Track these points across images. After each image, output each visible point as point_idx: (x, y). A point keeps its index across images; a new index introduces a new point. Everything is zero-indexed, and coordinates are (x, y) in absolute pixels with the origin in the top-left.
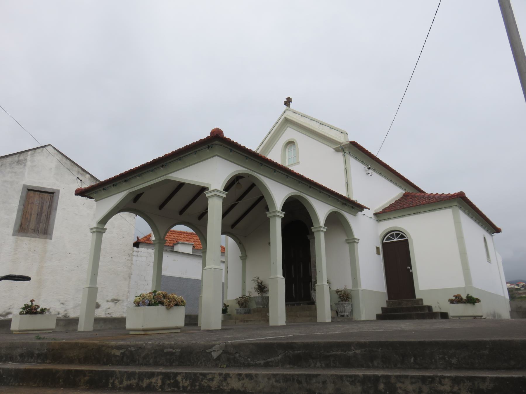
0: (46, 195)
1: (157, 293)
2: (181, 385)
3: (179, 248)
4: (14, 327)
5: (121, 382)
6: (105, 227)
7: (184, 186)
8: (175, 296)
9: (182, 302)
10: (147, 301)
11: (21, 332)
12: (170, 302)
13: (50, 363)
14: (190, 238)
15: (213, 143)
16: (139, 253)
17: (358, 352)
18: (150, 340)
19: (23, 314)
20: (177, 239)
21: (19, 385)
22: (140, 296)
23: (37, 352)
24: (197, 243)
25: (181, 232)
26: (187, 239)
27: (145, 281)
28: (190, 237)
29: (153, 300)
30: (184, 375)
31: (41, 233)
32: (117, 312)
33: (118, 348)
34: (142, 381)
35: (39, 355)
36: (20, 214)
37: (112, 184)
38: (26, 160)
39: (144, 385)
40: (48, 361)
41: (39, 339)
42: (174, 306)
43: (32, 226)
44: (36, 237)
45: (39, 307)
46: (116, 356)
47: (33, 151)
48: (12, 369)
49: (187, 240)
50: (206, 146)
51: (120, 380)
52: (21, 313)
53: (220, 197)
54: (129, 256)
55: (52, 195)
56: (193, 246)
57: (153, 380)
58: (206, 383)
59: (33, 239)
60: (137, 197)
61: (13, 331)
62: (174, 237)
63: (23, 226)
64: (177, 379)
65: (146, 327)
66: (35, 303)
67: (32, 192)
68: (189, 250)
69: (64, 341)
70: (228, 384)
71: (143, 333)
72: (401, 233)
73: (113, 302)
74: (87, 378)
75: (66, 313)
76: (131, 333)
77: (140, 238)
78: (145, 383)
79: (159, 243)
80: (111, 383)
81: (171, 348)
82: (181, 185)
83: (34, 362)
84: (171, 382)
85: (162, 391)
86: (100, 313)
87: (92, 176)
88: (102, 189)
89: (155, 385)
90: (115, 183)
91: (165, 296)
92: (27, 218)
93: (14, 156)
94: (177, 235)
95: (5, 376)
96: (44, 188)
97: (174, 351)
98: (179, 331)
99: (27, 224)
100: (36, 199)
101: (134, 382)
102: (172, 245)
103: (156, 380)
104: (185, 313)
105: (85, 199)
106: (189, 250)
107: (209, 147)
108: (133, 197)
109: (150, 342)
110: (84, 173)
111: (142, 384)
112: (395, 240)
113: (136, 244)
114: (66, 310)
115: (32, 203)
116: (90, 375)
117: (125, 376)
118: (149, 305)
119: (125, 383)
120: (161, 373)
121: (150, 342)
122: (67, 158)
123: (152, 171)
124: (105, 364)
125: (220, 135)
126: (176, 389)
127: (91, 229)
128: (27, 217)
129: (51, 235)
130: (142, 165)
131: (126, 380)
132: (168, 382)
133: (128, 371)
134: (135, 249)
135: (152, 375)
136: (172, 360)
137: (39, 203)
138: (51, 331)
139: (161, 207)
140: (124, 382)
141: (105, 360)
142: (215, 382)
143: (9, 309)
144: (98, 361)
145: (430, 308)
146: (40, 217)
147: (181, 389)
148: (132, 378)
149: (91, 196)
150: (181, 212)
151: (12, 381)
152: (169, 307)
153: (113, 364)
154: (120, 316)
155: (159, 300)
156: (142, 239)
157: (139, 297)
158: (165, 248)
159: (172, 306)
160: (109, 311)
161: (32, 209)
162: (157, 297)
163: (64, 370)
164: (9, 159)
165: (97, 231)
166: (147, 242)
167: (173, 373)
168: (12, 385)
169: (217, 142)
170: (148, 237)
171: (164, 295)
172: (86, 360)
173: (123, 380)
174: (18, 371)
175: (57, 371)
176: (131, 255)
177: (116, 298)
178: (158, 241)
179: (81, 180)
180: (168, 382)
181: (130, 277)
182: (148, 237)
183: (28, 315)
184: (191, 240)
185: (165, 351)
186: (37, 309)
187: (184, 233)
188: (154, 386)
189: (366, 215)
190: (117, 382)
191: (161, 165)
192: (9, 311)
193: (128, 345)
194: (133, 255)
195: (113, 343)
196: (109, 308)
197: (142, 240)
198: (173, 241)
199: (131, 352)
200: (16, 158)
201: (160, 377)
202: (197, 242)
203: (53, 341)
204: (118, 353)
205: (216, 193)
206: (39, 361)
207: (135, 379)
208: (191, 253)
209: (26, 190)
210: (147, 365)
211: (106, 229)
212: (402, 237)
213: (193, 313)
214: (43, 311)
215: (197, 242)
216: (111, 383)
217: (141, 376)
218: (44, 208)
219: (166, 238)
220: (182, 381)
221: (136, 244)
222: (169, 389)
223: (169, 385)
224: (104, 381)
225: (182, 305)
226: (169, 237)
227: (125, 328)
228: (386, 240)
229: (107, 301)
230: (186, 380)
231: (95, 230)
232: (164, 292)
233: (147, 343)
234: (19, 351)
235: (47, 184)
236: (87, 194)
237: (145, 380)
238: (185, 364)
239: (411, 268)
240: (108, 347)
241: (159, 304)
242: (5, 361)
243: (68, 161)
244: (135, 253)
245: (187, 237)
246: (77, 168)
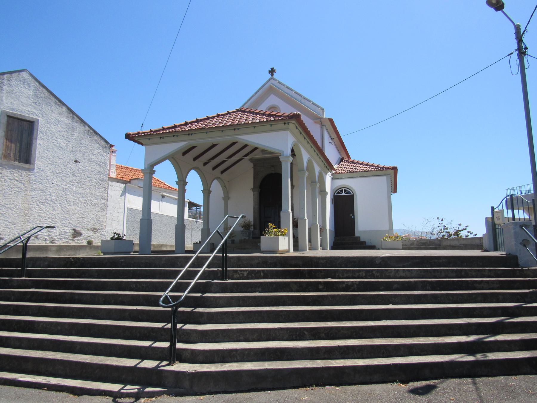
2: (375, 275)
17: (444, 260)
57: (361, 274)
58: (388, 274)
70: (398, 274)
72: (349, 190)
78: (356, 275)
89: (362, 276)
95: (269, 274)
112: (344, 194)
117: (345, 272)
122: (44, 87)
128: (8, 145)
132: (368, 274)
142: (392, 273)
145: (365, 242)
180: (368, 274)
188: (361, 276)
189: (143, 123)
201: (364, 272)
207: (351, 273)
212: (349, 193)
228: (336, 194)
230: (378, 273)
239: (354, 215)
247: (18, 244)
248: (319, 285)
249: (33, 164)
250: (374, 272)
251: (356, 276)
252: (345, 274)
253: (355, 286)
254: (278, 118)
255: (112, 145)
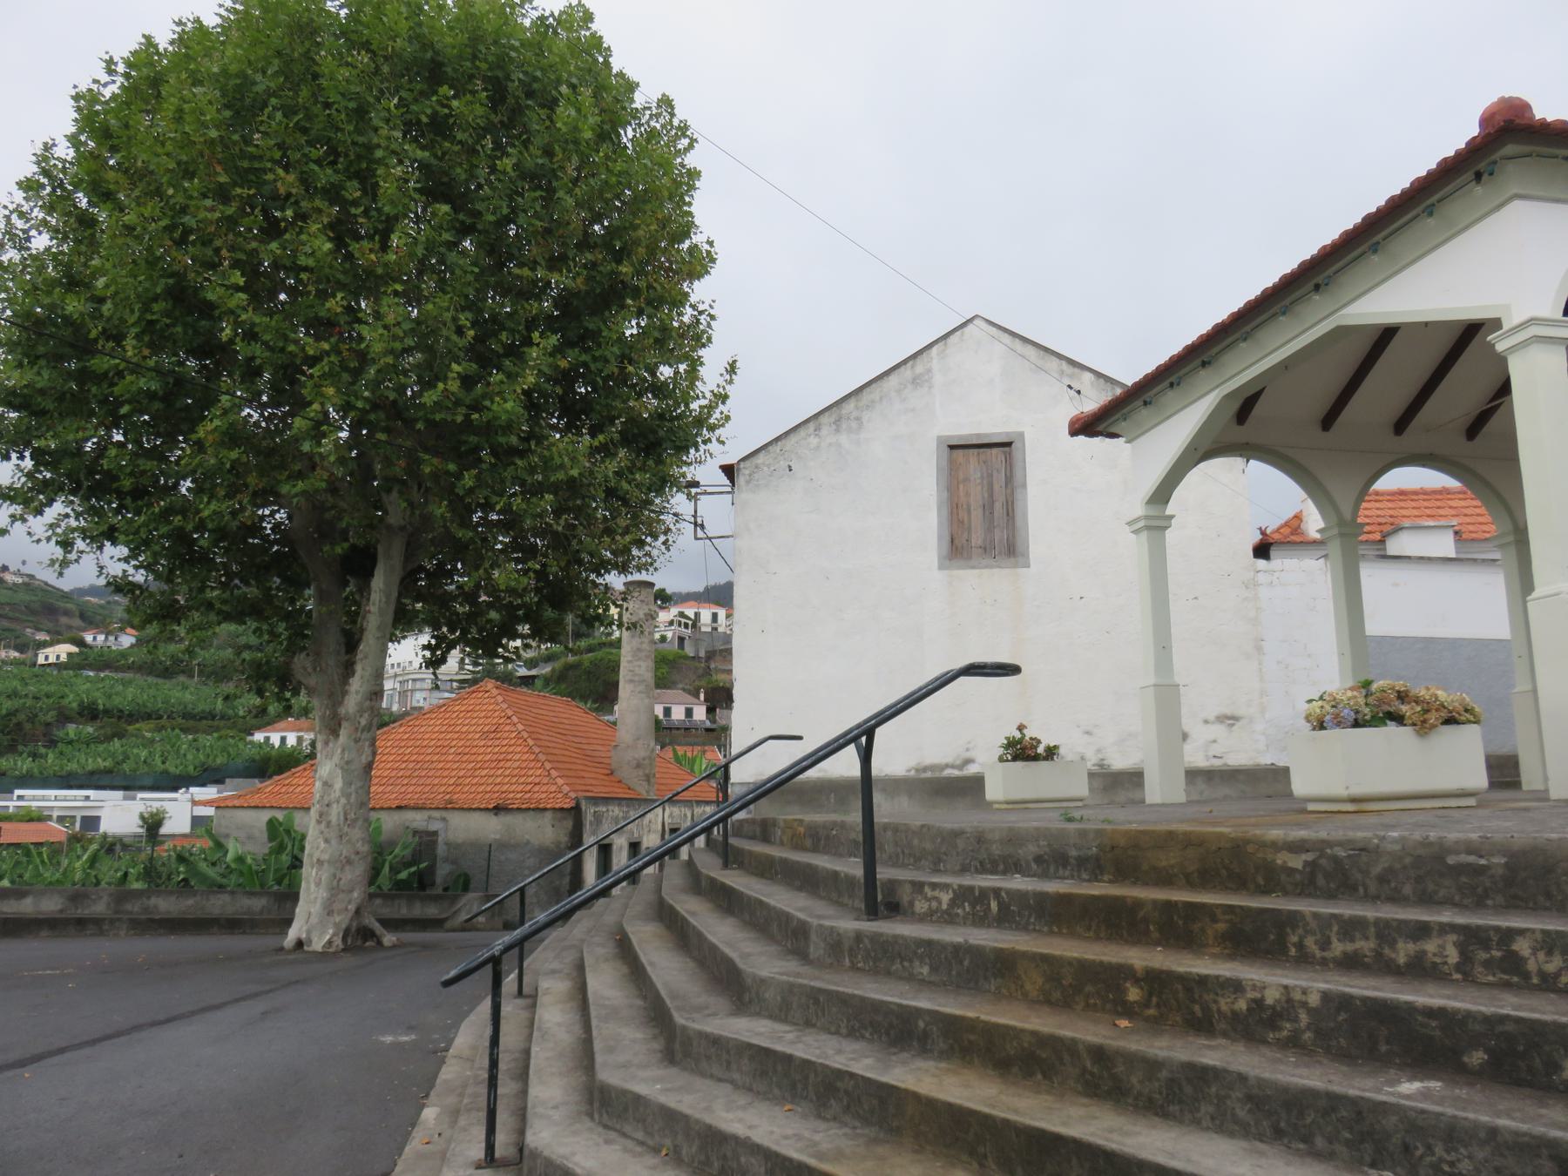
0: (995, 451)
1: (1374, 687)
2: (1532, 966)
3: (1400, 544)
4: (994, 791)
5: (1325, 944)
6: (1169, 512)
7: (1399, 334)
8: (1439, 693)
9: (1466, 711)
10: (1348, 714)
11: (1011, 806)
12: (1427, 711)
13: (1110, 882)
14: (1439, 508)
15: (1493, 158)
16: (1276, 574)
18: (1393, 827)
19: (1007, 761)
20: (1391, 516)
21: (1051, 932)
22: (1321, 698)
23: (1073, 853)
24: (1468, 520)
25: (1402, 493)
26: (1428, 512)
27: (1309, 656)
28: (1439, 504)
29: (1367, 710)
30: (1539, 936)
31: (1000, 553)
32: (1243, 751)
33: (1297, 847)
34: (1392, 944)
35: (1082, 862)
36: (945, 512)
37: (1166, 383)
38: (929, 371)
39: (1402, 960)
40: (1106, 878)
41: (1070, 820)
42: (1443, 723)
43: (977, 538)
44: (991, 567)
45: (1039, 742)
46: (1291, 871)
47: (941, 344)
48: (1027, 892)
49: (1428, 516)
50: (1470, 175)
51: (1319, 936)
52: (1001, 760)
53: (1554, 343)
54: (1247, 587)
55: (1007, 449)
56: (1456, 533)
57: (1430, 946)
59: (986, 572)
60: (1246, 406)
61: (990, 804)
62: (1379, 512)
63: (956, 541)
64: (1515, 947)
65: (1358, 790)
66: (1029, 733)
67: (960, 452)
68: (1443, 545)
69: (1134, 826)
71: (1350, 807)
73: (1222, 722)
74: (1221, 926)
75: (1100, 756)
76: (1311, 807)
77: (1268, 531)
78: (1402, 954)
79: (1342, 535)
80: (1294, 945)
81: (1469, 852)
82: (1387, 334)
83: (1072, 877)
84: (1492, 957)
85: (1464, 980)
86: (1196, 756)
87: (1098, 375)
88: (1139, 402)
89: (1438, 960)
90: (1173, 379)
91: (1402, 696)
92: (963, 522)
93: (902, 369)
94: (1390, 505)
96: (986, 435)
97: (1483, 862)
98: (1472, 802)
99: (965, 535)
100: (972, 464)
101: (1366, 946)
102: (1378, 536)
103: (1439, 946)
104: (1485, 747)
105: (1097, 440)
106: (1443, 545)
107: (1478, 177)
108: (1236, 405)
109: (1395, 834)
110: (1077, 370)
111: (1393, 956)
113: (1262, 550)
114: (1099, 751)
115: (966, 480)
116: (1227, 917)
117: (1335, 928)
118: (1357, 724)
119: (1338, 948)
120: (1453, 928)
121: (1396, 833)
123: (1284, 313)
124: (1265, 891)
125: (1517, 121)
126: (1515, 979)
127: (1129, 524)
129: (1026, 555)
130: (1249, 303)
131: (1339, 940)
133: (1341, 916)
134: (1261, 563)
135: (1422, 931)
136: (1480, 890)
137: (982, 478)
138: (1080, 804)
139: (1328, 421)
140: (1334, 946)
141: (1261, 881)
143: (968, 750)
144: (1240, 883)
146: (992, 513)
147: (1535, 981)
148: (1358, 935)
149: (1113, 430)
150: (1401, 426)
151: (1032, 920)
152: (1423, 727)
153: (1286, 893)
154: (1251, 763)
155: (1386, 708)
156: (1277, 531)
157: (1320, 703)
158: (1362, 550)
159: (1433, 727)
160: (1216, 749)
161: (967, 494)
162: (1379, 700)
163: (1155, 902)
164: (893, 380)
165: (1148, 528)
166: (1294, 538)
167: (1497, 929)
168: (1035, 930)
169: (1510, 149)
170: (1295, 523)
171: (1399, 692)
172: (1205, 877)
173: (1329, 937)
174: (1042, 897)
175: (1138, 904)
176: (1251, 585)
177: (1228, 712)
178: (1335, 531)
179: (1079, 392)
181: (1259, 649)
182: (1297, 521)
183: (1019, 764)
184: (1441, 512)
185: (1451, 860)
186: (1036, 747)
187: (1415, 493)
188: (1434, 964)
190: (1310, 943)
191: (1311, 285)
192: (968, 755)
193: (1323, 841)
194: (1256, 585)
195: (1276, 834)
196: (1215, 741)
197: (1277, 536)
198: (1380, 524)
199: (1336, 860)
200: (906, 372)
202: (1466, 515)
203: (1108, 827)
204: (1296, 862)
205: (1535, 330)
206: (1085, 876)
207: (1367, 938)
208: (1453, 555)
209: (947, 450)
210: (1396, 899)
211: (1172, 517)
213: (1505, 750)
214: (1051, 753)
215: (1466, 515)
216: (1294, 945)
217: (1387, 932)
218: (996, 487)
219: (1366, 509)
220: (1534, 954)
221: (1262, 550)
222: (1491, 978)
223: (1487, 964)
224: (1272, 937)
225: (1470, 722)
226: (1369, 512)
227: (1290, 795)
229: (1206, 722)
230: (1550, 953)
231: (1141, 524)
232: (1400, 685)
233: (1384, 837)
234: (1032, 849)
235: (989, 425)
236: (1100, 428)
237: (1400, 945)
238: (1531, 905)
240: (1263, 845)
241: (1388, 722)
242: (1004, 873)
243: (1030, 347)
244: (1261, 578)
245: (1426, 504)
246: (1054, 363)
247: (812, 773)
248: (1128, 985)
249: (1023, 555)
250: (1522, 947)
251: (1402, 960)
252: (1334, 940)
253: (1304, 1018)
254: (80, 643)
255: (396, 613)
